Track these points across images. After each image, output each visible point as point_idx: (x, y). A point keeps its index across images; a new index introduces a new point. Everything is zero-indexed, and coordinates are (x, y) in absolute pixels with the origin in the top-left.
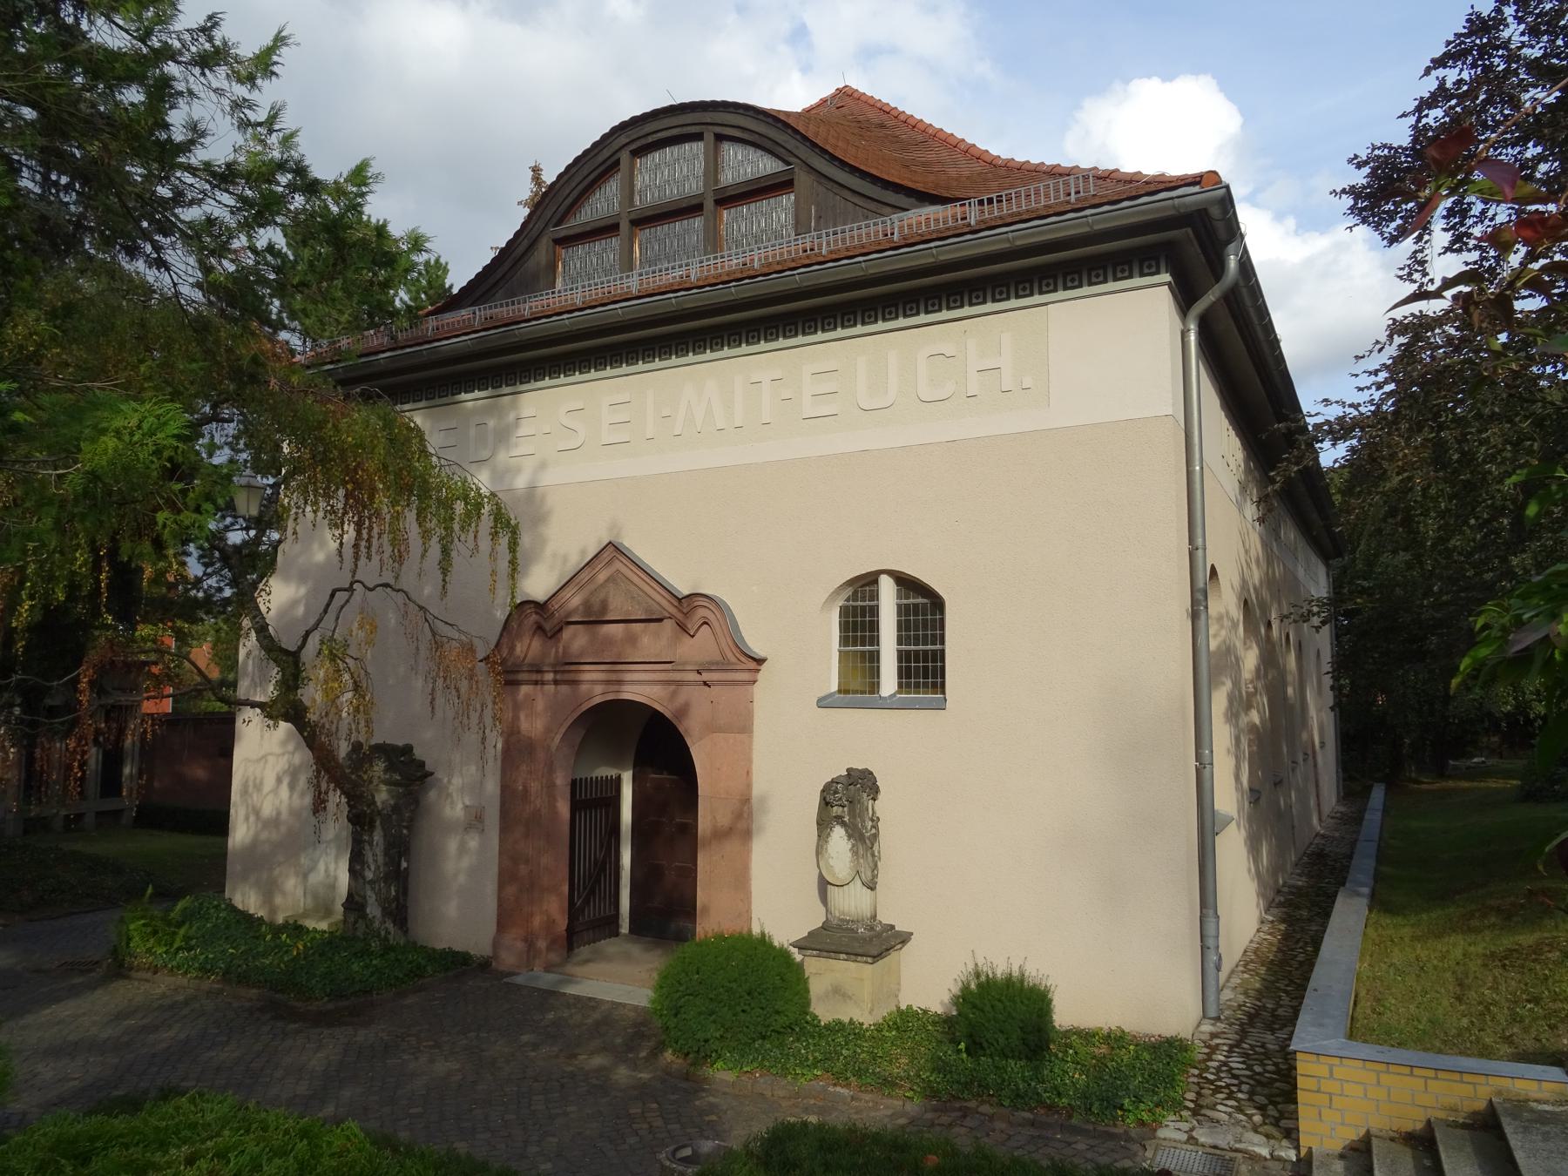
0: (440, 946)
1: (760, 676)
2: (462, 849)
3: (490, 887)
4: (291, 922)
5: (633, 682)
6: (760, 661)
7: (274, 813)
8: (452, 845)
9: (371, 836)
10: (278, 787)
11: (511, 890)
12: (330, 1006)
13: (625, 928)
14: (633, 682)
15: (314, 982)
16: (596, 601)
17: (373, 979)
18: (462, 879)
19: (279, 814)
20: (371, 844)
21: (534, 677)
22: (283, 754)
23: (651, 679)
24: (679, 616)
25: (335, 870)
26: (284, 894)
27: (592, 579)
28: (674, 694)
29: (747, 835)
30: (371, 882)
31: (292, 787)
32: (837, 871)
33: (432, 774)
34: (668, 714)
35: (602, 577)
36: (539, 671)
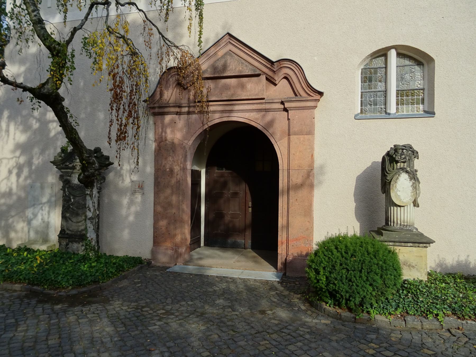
0: (121, 254)
1: (319, 104)
2: (131, 203)
3: (149, 222)
4: (22, 247)
5: (239, 111)
6: (321, 94)
7: (8, 190)
8: (125, 201)
9: (92, 191)
10: (9, 176)
11: (163, 223)
12: (74, 292)
13: (202, 244)
14: (239, 111)
15: (60, 278)
16: (220, 64)
17: (98, 274)
18: (131, 218)
19: (11, 190)
20: (91, 196)
21: (177, 110)
22: (12, 158)
23: (251, 108)
24: (270, 73)
25: (48, 218)
26: (16, 231)
27: (215, 53)
28: (264, 116)
29: (312, 186)
30: (91, 219)
31: (18, 175)
32: (402, 198)
33: (113, 164)
34: (259, 127)
35: (220, 54)
36: (180, 107)
